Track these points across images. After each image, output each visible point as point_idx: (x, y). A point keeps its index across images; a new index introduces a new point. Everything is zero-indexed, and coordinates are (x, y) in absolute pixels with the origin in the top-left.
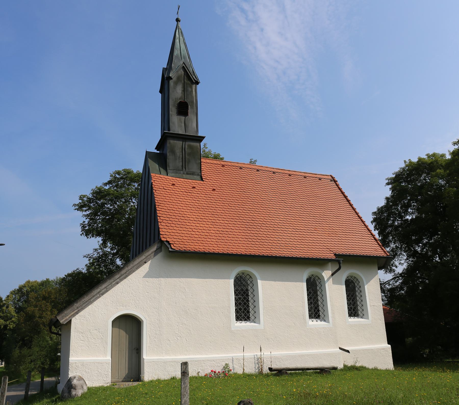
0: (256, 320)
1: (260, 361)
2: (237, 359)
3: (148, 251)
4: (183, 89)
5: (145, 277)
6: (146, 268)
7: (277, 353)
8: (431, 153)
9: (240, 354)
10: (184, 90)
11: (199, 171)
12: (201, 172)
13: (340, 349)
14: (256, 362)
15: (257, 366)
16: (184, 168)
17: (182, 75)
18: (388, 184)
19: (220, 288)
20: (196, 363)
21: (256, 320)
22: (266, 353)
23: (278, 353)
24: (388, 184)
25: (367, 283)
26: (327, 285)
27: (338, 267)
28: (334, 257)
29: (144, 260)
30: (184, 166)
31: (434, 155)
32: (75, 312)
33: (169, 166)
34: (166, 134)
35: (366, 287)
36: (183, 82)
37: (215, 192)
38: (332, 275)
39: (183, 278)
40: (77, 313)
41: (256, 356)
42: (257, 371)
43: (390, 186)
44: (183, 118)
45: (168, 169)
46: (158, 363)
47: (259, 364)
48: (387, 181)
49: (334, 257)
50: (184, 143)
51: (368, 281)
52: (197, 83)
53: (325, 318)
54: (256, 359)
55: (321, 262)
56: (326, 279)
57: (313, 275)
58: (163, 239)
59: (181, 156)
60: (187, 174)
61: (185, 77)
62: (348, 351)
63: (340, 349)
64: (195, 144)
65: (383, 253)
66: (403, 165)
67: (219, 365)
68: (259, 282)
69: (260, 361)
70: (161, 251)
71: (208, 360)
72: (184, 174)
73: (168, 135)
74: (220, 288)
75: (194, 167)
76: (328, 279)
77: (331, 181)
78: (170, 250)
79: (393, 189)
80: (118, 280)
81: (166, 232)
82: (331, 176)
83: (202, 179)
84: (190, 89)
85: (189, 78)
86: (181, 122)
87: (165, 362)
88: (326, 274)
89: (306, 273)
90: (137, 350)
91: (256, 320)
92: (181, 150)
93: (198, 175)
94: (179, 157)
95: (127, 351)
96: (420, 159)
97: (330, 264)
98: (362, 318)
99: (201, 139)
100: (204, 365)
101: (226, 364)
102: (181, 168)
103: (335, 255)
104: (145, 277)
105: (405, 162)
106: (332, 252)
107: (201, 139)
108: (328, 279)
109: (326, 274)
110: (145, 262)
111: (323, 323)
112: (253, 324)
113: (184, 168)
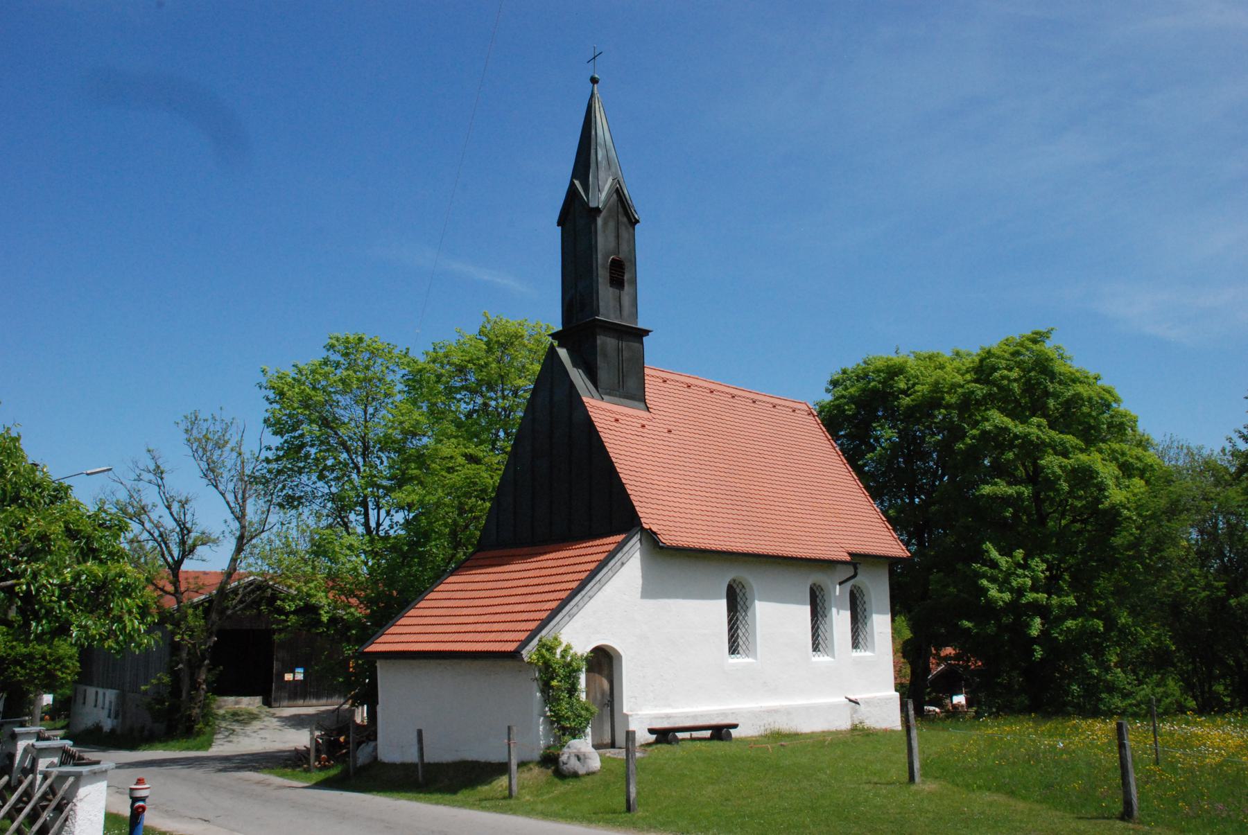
28: (848, 558)
49: (848, 558)
52: (637, 221)
58: (646, 526)
81: (649, 517)
89: (818, 577)
91: (751, 652)
103: (850, 554)
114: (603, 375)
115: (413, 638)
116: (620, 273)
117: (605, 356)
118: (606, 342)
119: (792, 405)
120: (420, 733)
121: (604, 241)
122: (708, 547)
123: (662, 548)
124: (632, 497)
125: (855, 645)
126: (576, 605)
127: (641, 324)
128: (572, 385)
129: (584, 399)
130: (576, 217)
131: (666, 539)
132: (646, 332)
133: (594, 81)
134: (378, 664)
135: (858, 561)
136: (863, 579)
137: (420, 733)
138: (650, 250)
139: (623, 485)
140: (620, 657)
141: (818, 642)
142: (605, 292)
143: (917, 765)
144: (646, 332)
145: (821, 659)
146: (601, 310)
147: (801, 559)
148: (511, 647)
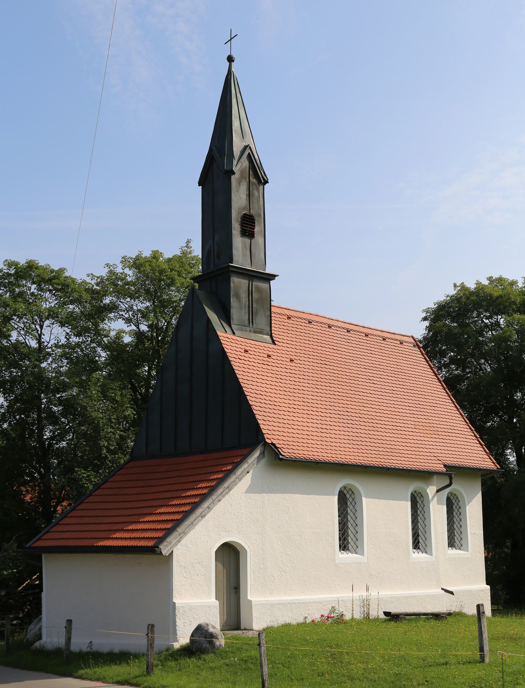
0: (358, 550)
1: (366, 603)
2: (343, 601)
3: (251, 457)
4: (248, 193)
5: (247, 492)
6: (247, 480)
7: (385, 593)
8: (495, 276)
9: (347, 595)
10: (249, 195)
11: (269, 329)
12: (271, 330)
13: (442, 589)
14: (362, 604)
15: (363, 610)
16: (251, 323)
17: (246, 168)
18: (425, 319)
19: (320, 506)
20: (303, 605)
21: (358, 549)
22: (373, 593)
23: (200, 601)
24: (425, 319)
25: (469, 504)
26: (431, 505)
27: (448, 482)
28: (444, 470)
29: (246, 470)
30: (251, 320)
31: (500, 280)
32: (177, 539)
33: (233, 319)
34: (230, 269)
35: (467, 508)
36: (248, 180)
37: (294, 364)
38: (438, 491)
39: (286, 493)
40: (179, 541)
41: (361, 597)
42: (362, 616)
43: (427, 323)
44: (248, 241)
45: (232, 323)
46: (269, 604)
47: (364, 608)
48: (424, 315)
49: (444, 470)
50: (251, 283)
51: (470, 501)
52: (266, 182)
53: (427, 549)
54: (362, 601)
55: (426, 475)
56: (430, 498)
57: (415, 491)
58: (268, 441)
59: (247, 303)
60: (255, 332)
61: (251, 172)
62: (452, 593)
63: (442, 589)
64: (263, 285)
65: (493, 464)
66: (452, 292)
67: (325, 608)
68: (364, 499)
69: (366, 603)
70: (264, 456)
71: (315, 602)
72: (250, 332)
73: (233, 269)
74: (320, 506)
75: (261, 321)
76: (433, 498)
77: (414, 346)
78: (281, 457)
79: (429, 328)
80: (220, 497)
81: (271, 431)
82: (412, 337)
83: (274, 342)
84: (256, 193)
85: (256, 176)
86: (246, 248)
87: (273, 605)
88: (431, 490)
89: (413, 486)
90: (236, 589)
91: (358, 549)
92: (247, 294)
93: (267, 334)
94: (245, 306)
95: (225, 591)
96: (478, 283)
97: (435, 477)
98: (460, 549)
99: (269, 278)
100: (311, 608)
101: (333, 607)
102: (247, 322)
103: (445, 466)
104: (247, 492)
105: (455, 286)
106: (440, 462)
107: (269, 278)
108: (433, 498)
109: (431, 490)
110: (248, 472)
111: (425, 555)
112: (354, 555)
113: (251, 323)
114: (235, 313)
115: (73, 535)
116: (249, 225)
117: (238, 296)
118: (238, 283)
119: (399, 338)
120: (69, 622)
121: (239, 199)
122: (389, 465)
123: (281, 459)
124: (257, 416)
125: (451, 544)
126: (209, 508)
127: (268, 271)
128: (209, 321)
129: (219, 333)
130: (216, 176)
131: (286, 452)
132: (273, 277)
133: (230, 59)
134: (43, 555)
135: (454, 472)
136: (457, 487)
137: (69, 622)
138: (277, 207)
139: (250, 405)
140: (246, 551)
141: (418, 541)
142: (238, 242)
143: (485, 635)
144: (273, 277)
145: (418, 556)
146: (235, 258)
147: (403, 470)
148: (151, 543)
